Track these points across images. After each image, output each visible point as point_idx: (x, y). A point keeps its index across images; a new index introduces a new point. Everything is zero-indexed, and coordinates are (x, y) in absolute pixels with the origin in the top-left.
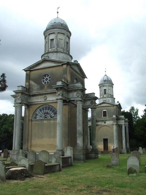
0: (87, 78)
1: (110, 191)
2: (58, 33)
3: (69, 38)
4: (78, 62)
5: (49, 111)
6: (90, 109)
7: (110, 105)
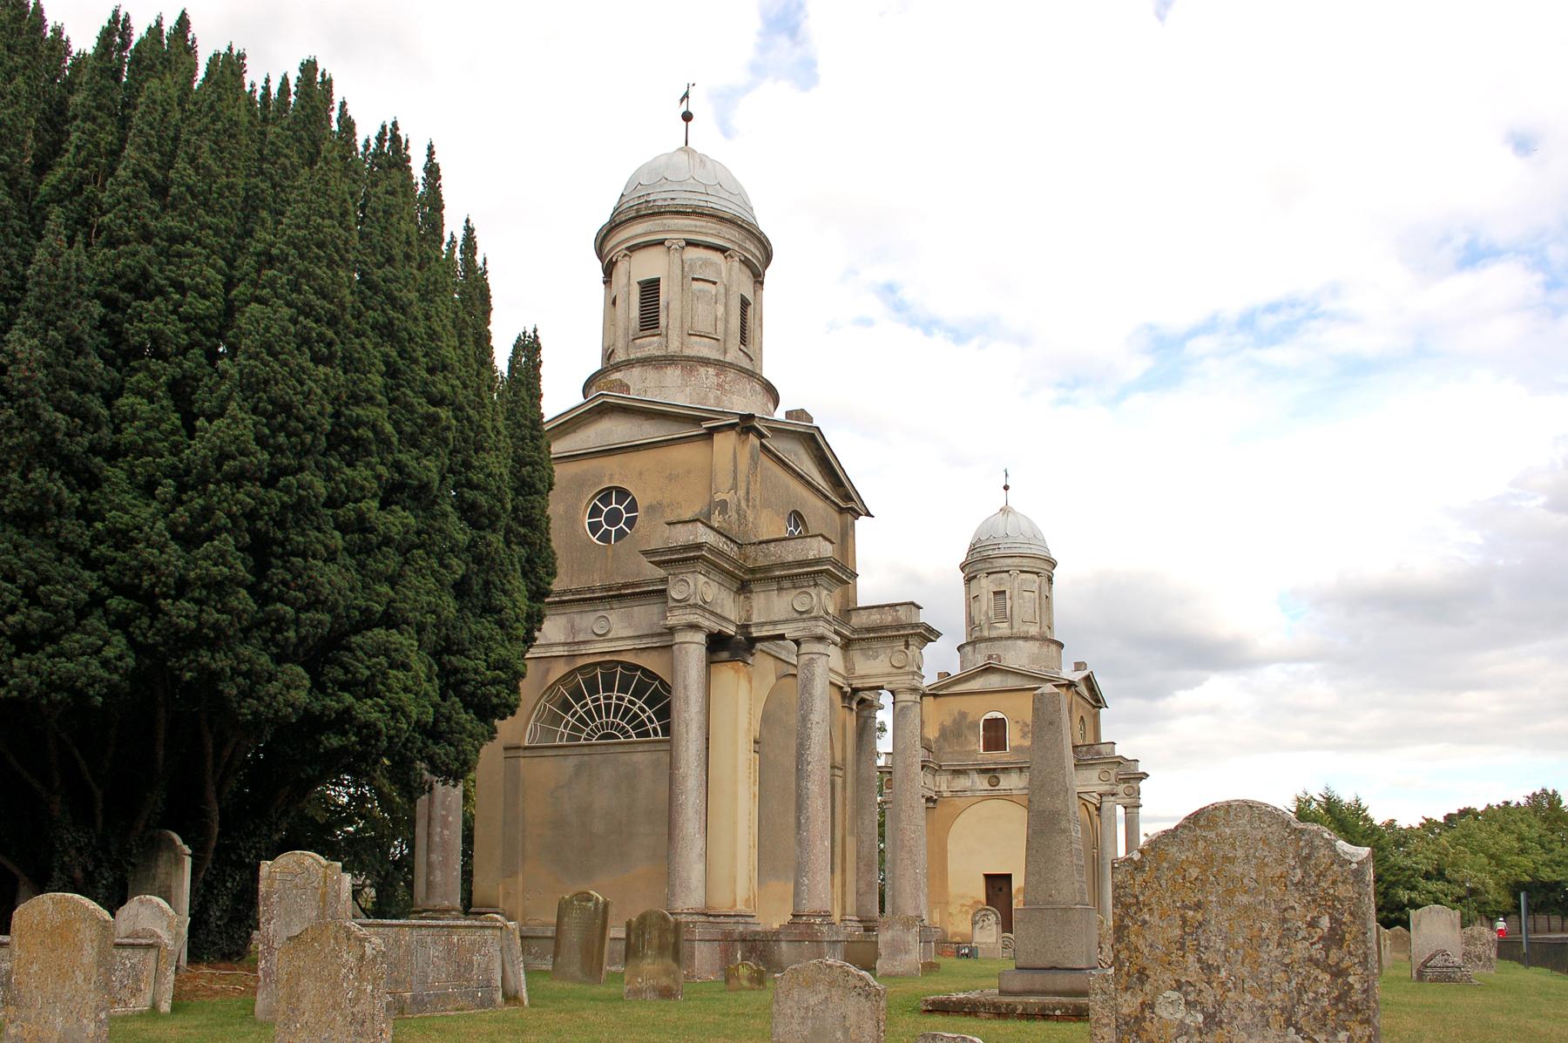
0: (868, 514)
1: (250, 358)
2: (689, 243)
3: (758, 279)
4: (810, 419)
5: (650, 712)
6: (886, 698)
7: (1012, 682)
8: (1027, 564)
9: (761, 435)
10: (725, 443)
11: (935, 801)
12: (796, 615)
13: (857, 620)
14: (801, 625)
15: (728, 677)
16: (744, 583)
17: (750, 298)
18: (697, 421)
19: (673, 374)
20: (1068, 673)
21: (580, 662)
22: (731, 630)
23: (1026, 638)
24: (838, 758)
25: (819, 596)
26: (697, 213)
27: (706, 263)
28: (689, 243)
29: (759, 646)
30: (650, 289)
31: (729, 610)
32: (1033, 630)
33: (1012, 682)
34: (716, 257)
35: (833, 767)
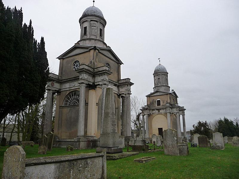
0: (123, 64)
2: (91, 20)
7: (161, 94)
8: (163, 73)
9: (98, 50)
10: (92, 51)
11: (150, 115)
12: (101, 80)
13: (120, 82)
14: (102, 82)
15: (92, 92)
16: (94, 75)
17: (102, 29)
18: (87, 48)
19: (87, 41)
20: (171, 92)
21: (71, 91)
22: (91, 84)
23: (163, 86)
24: (117, 107)
25: (105, 77)
26: (92, 15)
27: (94, 23)
28: (91, 20)
29: (97, 86)
30: (85, 28)
31: (91, 79)
32: (165, 85)
33: (161, 94)
34: (96, 22)
35: (116, 108)
